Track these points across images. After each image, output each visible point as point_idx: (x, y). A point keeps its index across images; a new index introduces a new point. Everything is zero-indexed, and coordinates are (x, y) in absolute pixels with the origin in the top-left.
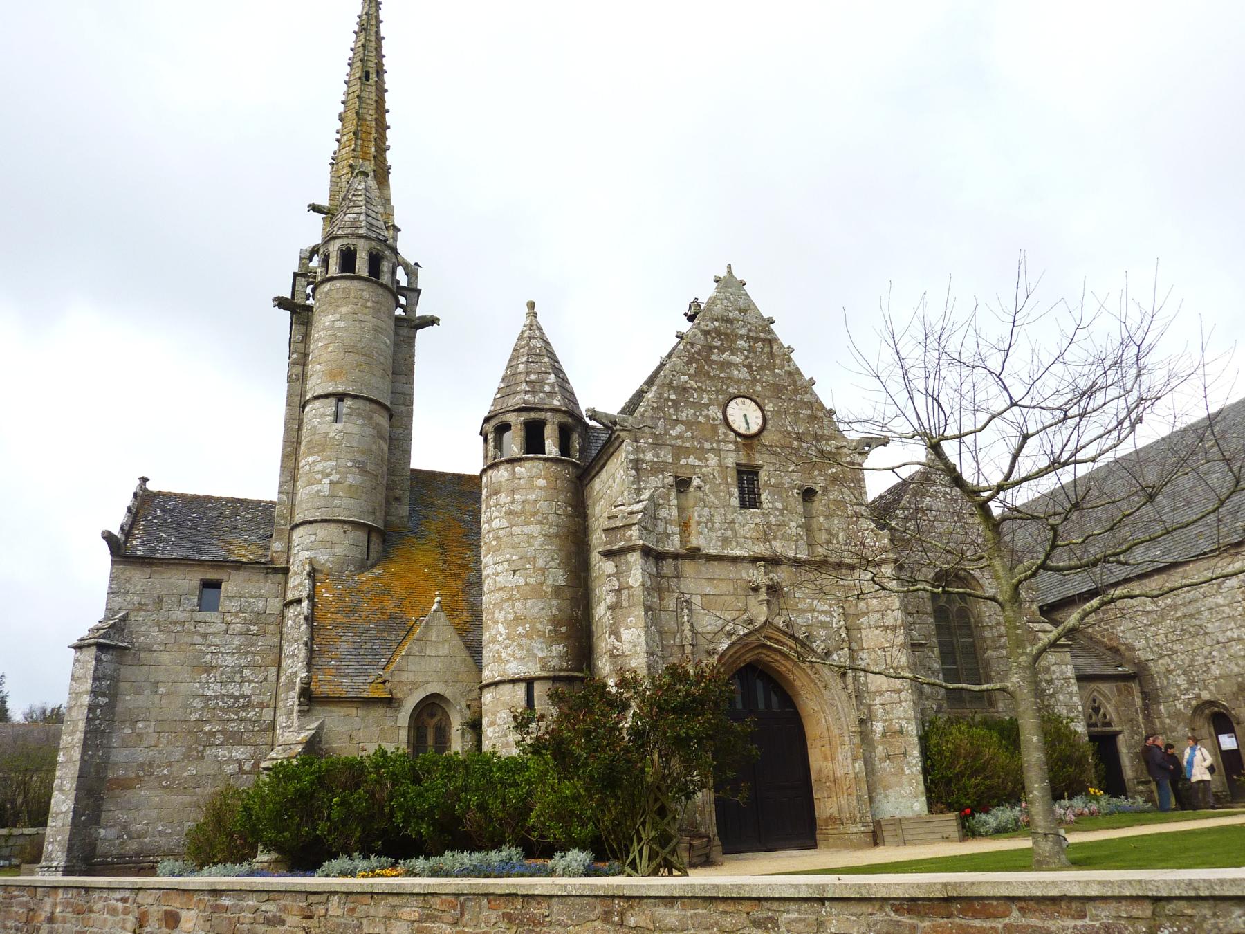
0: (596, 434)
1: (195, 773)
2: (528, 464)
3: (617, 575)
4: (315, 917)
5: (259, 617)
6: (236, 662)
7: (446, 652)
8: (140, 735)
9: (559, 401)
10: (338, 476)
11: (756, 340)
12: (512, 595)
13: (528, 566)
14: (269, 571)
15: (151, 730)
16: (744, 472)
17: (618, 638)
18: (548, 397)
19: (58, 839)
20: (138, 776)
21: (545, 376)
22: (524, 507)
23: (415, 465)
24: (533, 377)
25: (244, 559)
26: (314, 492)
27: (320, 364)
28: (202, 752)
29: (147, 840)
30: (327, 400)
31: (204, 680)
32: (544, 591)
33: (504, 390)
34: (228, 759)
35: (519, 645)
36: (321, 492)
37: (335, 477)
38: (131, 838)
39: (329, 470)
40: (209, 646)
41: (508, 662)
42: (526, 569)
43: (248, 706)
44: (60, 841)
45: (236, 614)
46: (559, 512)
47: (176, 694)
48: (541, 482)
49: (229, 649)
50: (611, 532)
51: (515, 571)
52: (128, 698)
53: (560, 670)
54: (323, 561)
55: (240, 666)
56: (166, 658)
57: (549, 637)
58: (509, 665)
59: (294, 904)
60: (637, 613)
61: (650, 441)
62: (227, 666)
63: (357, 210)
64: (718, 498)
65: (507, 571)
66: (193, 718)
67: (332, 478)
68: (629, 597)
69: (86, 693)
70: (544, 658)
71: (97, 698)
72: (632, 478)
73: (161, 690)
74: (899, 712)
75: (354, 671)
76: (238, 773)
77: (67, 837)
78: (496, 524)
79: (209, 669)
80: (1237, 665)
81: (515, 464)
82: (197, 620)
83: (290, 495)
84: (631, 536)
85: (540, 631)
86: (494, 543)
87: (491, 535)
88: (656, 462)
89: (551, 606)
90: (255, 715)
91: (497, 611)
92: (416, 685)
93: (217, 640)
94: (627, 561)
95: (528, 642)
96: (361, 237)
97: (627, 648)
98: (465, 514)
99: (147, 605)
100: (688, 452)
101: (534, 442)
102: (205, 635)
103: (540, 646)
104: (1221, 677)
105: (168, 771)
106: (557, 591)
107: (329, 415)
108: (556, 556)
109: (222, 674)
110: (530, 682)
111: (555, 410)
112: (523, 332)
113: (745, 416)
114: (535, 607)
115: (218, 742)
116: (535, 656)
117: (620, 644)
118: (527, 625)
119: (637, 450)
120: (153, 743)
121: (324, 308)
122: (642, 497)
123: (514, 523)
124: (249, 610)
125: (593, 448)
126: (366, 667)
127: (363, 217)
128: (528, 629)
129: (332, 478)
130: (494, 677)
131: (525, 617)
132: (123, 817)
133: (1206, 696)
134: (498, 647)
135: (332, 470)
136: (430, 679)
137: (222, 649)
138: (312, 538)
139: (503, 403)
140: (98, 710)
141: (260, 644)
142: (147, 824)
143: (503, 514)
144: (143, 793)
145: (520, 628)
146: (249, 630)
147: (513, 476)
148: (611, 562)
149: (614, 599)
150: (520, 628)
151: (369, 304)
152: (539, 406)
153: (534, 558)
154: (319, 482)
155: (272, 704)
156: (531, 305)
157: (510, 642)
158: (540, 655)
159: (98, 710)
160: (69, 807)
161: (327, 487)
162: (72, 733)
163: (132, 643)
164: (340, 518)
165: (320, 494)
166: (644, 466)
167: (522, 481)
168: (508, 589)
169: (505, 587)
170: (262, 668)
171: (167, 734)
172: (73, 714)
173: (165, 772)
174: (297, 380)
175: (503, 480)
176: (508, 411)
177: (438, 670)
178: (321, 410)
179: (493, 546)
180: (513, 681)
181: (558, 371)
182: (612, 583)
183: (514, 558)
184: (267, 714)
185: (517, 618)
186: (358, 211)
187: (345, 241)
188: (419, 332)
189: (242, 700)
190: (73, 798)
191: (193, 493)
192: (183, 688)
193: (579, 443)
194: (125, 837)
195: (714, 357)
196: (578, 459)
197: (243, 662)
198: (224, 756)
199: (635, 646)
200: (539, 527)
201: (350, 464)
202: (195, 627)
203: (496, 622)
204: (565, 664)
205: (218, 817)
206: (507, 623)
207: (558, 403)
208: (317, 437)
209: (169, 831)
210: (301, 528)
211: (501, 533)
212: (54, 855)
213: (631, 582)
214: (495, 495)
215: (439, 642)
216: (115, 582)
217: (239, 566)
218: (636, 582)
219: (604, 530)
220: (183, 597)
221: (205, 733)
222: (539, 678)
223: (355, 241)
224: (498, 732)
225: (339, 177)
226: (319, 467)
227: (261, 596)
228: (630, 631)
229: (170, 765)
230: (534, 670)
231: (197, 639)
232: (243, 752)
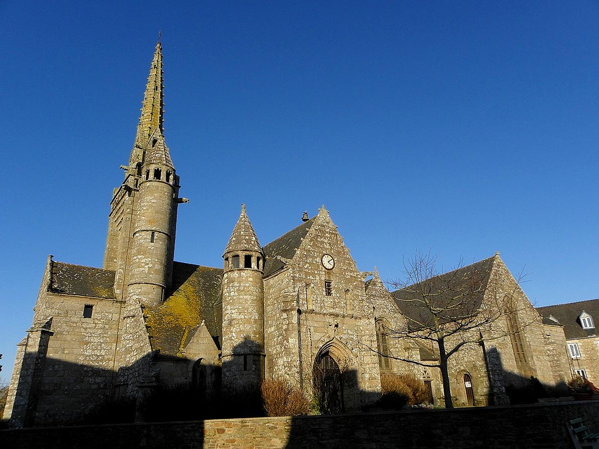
5: (109, 322)
8: (56, 371)
11: (332, 234)
16: (327, 282)
17: (288, 342)
19: (19, 417)
24: (247, 237)
28: (82, 379)
37: (150, 265)
45: (99, 320)
47: (73, 354)
56: (69, 338)
64: (319, 291)
73: (66, 352)
74: (374, 371)
76: (97, 389)
79: (87, 343)
80: (473, 358)
100: (309, 274)
101: (248, 264)
102: (86, 329)
104: (468, 362)
106: (255, 321)
113: (327, 262)
119: (294, 273)
120: (61, 375)
127: (164, 156)
129: (149, 265)
133: (462, 368)
141: (109, 333)
146: (105, 327)
151: (166, 194)
154: (144, 267)
167: (244, 278)
173: (66, 388)
183: (240, 308)
185: (240, 331)
187: (157, 166)
192: (75, 351)
195: (319, 239)
198: (92, 381)
201: (156, 260)
205: (408, 376)
209: (67, 413)
220: (77, 312)
222: (249, 354)
225: (144, 131)
226: (143, 261)
227: (110, 313)
231: (82, 330)
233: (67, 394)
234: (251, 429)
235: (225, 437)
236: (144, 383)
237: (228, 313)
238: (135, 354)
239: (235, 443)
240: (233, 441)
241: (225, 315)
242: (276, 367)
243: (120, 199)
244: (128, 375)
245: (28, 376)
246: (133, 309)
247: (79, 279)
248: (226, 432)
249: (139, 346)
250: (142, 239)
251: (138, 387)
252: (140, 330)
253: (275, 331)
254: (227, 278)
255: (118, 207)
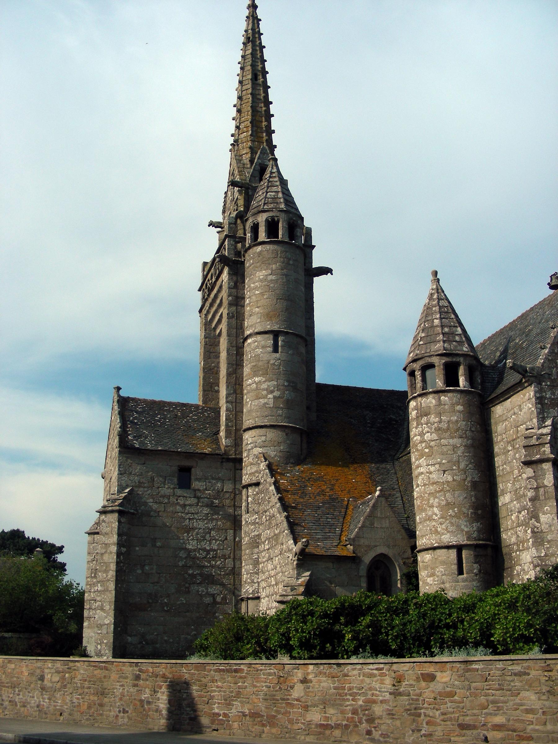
0: (486, 371)
1: (184, 602)
2: (449, 395)
3: (535, 478)
4: (554, 671)
6: (206, 525)
7: (388, 525)
9: (466, 348)
10: (279, 393)
12: (443, 488)
13: (454, 468)
14: (224, 460)
15: (154, 571)
17: (538, 521)
18: (459, 345)
19: (105, 641)
20: (148, 602)
21: (454, 329)
22: (449, 425)
23: (317, 381)
24: (446, 330)
25: (206, 451)
26: (261, 404)
27: (258, 307)
29: (158, 646)
30: (267, 336)
31: (185, 538)
32: (466, 485)
33: (425, 339)
34: (206, 594)
35: (451, 523)
36: (268, 404)
38: (147, 643)
39: (272, 388)
40: (187, 514)
41: (443, 534)
42: (453, 470)
43: (216, 557)
44: (106, 644)
46: (473, 429)
48: (459, 408)
49: (200, 516)
50: (529, 448)
51: (444, 471)
52: (137, 549)
53: (479, 540)
54: (272, 456)
55: (208, 528)
57: (471, 517)
58: (444, 536)
59: (536, 665)
60: (551, 504)
61: (548, 383)
62: (200, 529)
63: (274, 189)
65: (438, 470)
66: (181, 564)
67: (274, 394)
68: (545, 493)
69: (114, 544)
70: (469, 532)
71: (120, 548)
72: (539, 410)
73: (159, 544)
75: (321, 537)
77: (112, 640)
78: (427, 437)
81: (441, 394)
82: (178, 494)
83: (234, 404)
84: (544, 451)
85: (464, 513)
86: (427, 450)
87: (423, 445)
88: (553, 399)
89: (471, 496)
90: (221, 563)
91: (432, 499)
92: (370, 548)
93: (192, 510)
94: (542, 468)
95: (458, 520)
96: (282, 211)
97: (544, 527)
98: (351, 418)
99: (144, 483)
102: (184, 506)
103: (465, 523)
105: (167, 600)
107: (269, 347)
108: (472, 461)
109: (197, 534)
110: (459, 548)
111: (465, 356)
112: (432, 295)
114: (460, 496)
115: (198, 582)
116: (462, 530)
117: (539, 524)
118: (456, 509)
121: (258, 264)
122: (546, 423)
123: (442, 436)
124: (212, 488)
125: (487, 381)
126: (329, 534)
127: (280, 195)
128: (456, 512)
129: (274, 394)
130: (432, 543)
131: (454, 503)
132: (142, 630)
134: (434, 523)
135: (274, 388)
136: (378, 544)
137: (196, 516)
138: (263, 438)
139: (427, 348)
140: (122, 556)
141: (221, 513)
142: (157, 635)
143: (433, 430)
144: (152, 614)
145: (451, 511)
146: (213, 503)
147: (440, 403)
148: (531, 469)
149: (533, 494)
150: (451, 511)
151: (291, 262)
152: (454, 352)
153: (459, 462)
154: (265, 397)
155: (232, 555)
156: (435, 273)
157: (444, 520)
158: (466, 529)
159: (122, 556)
160: (111, 621)
161: (271, 401)
162: (106, 571)
163: (136, 510)
164: (282, 424)
165: (267, 406)
166: (546, 401)
168: (440, 484)
169: (437, 482)
170: (224, 531)
171: (164, 575)
172: (104, 558)
173: (166, 600)
174: (233, 317)
175: (432, 405)
176: (433, 355)
177: (383, 537)
178: (263, 343)
179: (426, 453)
180: (448, 547)
181: (461, 325)
182: (531, 483)
183: (444, 461)
184: (229, 563)
185: (448, 504)
186: (276, 190)
188: (316, 279)
189: (211, 553)
190: (113, 616)
191: (151, 399)
193: (479, 379)
194: (144, 643)
196: (480, 390)
197: (210, 526)
198: (203, 592)
199: (550, 526)
200: (460, 440)
202: (177, 500)
203: (432, 506)
204: (482, 536)
206: (439, 506)
207: (467, 350)
208: (260, 363)
210: (253, 430)
211: (432, 444)
212: (103, 652)
213: (546, 482)
214: (425, 416)
215: (383, 518)
216: (122, 466)
217: (203, 456)
218: (550, 483)
219: (524, 447)
221: (189, 575)
223: (278, 214)
224: (437, 581)
228: (547, 516)
229: (168, 596)
230: (461, 539)
232: (215, 589)
233: (167, 611)
234: (482, 676)
235: (435, 687)
236: (287, 596)
237: (422, 473)
238: (267, 547)
239: (456, 698)
240: (451, 694)
241: (417, 477)
242: (518, 568)
243: (214, 280)
244: (258, 583)
245: (109, 580)
246: (256, 472)
247: (164, 423)
248: (438, 678)
249: (272, 534)
250: (257, 347)
251: (278, 602)
252: (272, 507)
253: (512, 501)
254: (416, 408)
255: (212, 295)
